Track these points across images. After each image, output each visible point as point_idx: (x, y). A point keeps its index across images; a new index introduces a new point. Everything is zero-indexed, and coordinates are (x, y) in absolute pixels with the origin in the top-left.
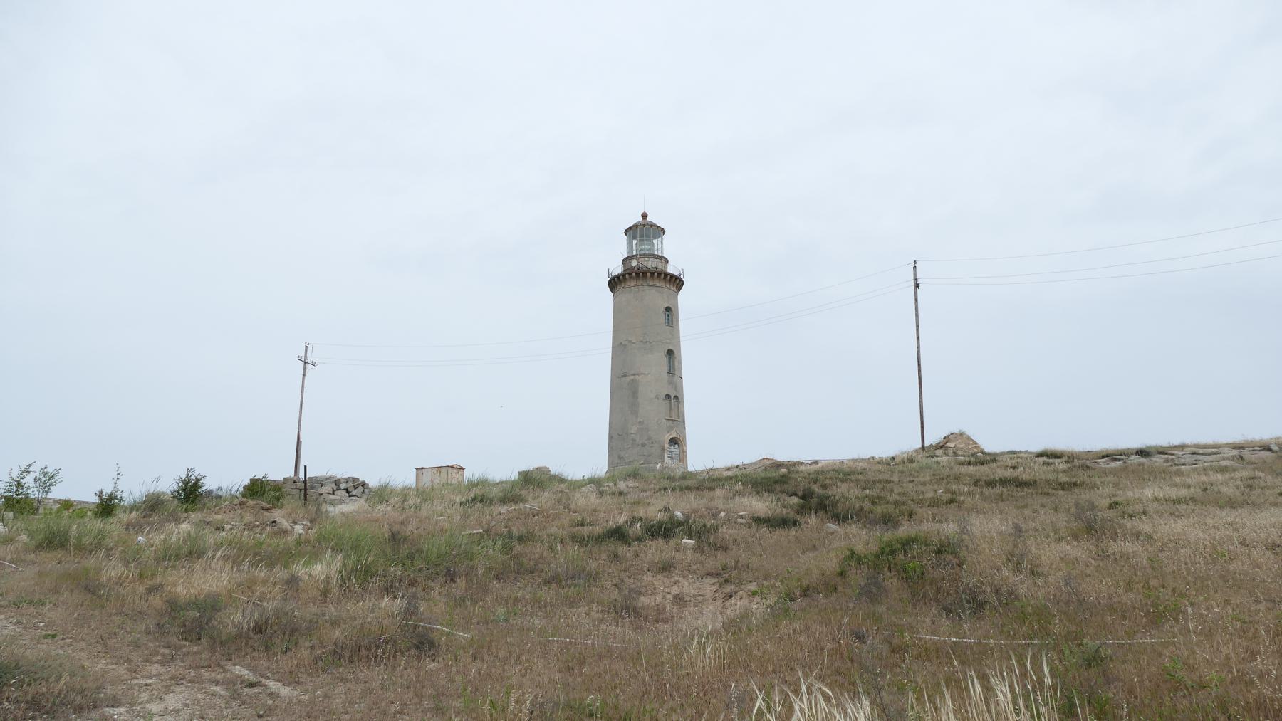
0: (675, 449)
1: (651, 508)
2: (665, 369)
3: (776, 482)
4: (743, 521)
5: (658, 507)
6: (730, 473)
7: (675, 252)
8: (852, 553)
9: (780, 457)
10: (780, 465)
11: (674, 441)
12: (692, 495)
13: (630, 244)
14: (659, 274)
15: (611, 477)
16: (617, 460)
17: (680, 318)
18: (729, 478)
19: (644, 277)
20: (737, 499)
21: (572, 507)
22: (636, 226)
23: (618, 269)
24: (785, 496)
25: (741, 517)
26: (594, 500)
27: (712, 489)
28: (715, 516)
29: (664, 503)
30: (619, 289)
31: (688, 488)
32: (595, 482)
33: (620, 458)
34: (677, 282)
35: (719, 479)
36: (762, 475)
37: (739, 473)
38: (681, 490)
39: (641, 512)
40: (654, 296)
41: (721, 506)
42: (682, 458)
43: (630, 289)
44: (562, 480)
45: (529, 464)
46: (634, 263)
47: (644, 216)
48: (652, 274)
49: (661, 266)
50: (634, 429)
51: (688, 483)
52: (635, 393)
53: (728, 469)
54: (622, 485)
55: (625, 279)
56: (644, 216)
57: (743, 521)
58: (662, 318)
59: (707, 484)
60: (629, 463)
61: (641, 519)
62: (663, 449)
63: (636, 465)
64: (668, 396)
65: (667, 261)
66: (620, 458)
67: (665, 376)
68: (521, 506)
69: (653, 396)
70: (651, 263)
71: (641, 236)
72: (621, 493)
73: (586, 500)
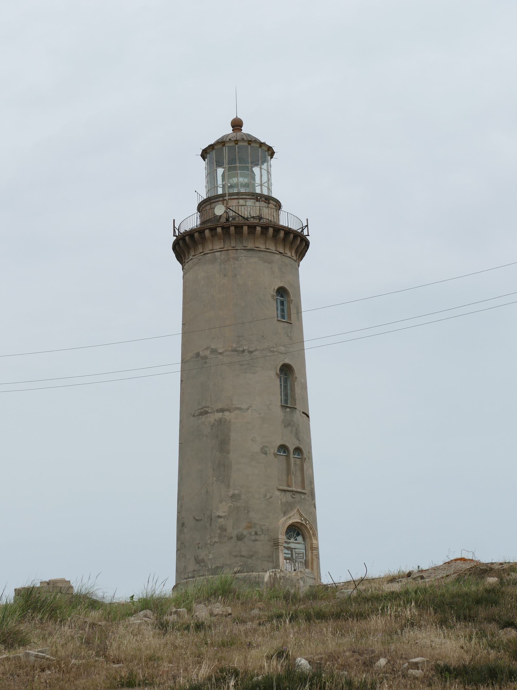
0: (298, 545)
1: (254, 652)
2: (277, 399)
3: (478, 602)
4: (418, 673)
5: (266, 650)
6: (396, 587)
7: (293, 189)
8: (310, 586)
9: (486, 556)
10: (483, 570)
11: (295, 530)
12: (327, 628)
13: (211, 176)
14: (265, 228)
15: (182, 597)
16: (192, 566)
17: (305, 306)
18: (393, 596)
19: (238, 236)
20: (410, 634)
21: (112, 652)
22: (221, 143)
23: (191, 221)
24: (492, 627)
25: (416, 665)
26: (151, 640)
27: (361, 616)
28: (369, 664)
29: (277, 643)
30: (193, 258)
31: (321, 616)
32: (151, 605)
33: (198, 561)
34: (297, 243)
35: (376, 598)
36: (454, 589)
37: (412, 585)
38: (309, 618)
39: (236, 660)
40: (256, 269)
41: (378, 648)
42: (310, 560)
43: (214, 258)
44: (94, 604)
45: (34, 574)
46: (219, 210)
47: (237, 125)
48: (252, 228)
49: (267, 213)
50: (222, 509)
51: (322, 605)
52: (223, 444)
53: (392, 580)
54: (202, 612)
55: (203, 239)
56: (237, 125)
57: (418, 673)
58: (272, 308)
59: (354, 608)
60: (215, 571)
61: (236, 673)
62: (276, 544)
63: (227, 574)
64: (283, 448)
65: (278, 205)
66: (198, 561)
67: (278, 412)
68: (20, 652)
69: (256, 448)
70: (249, 209)
71: (232, 161)
72: (199, 626)
73: (138, 639)
